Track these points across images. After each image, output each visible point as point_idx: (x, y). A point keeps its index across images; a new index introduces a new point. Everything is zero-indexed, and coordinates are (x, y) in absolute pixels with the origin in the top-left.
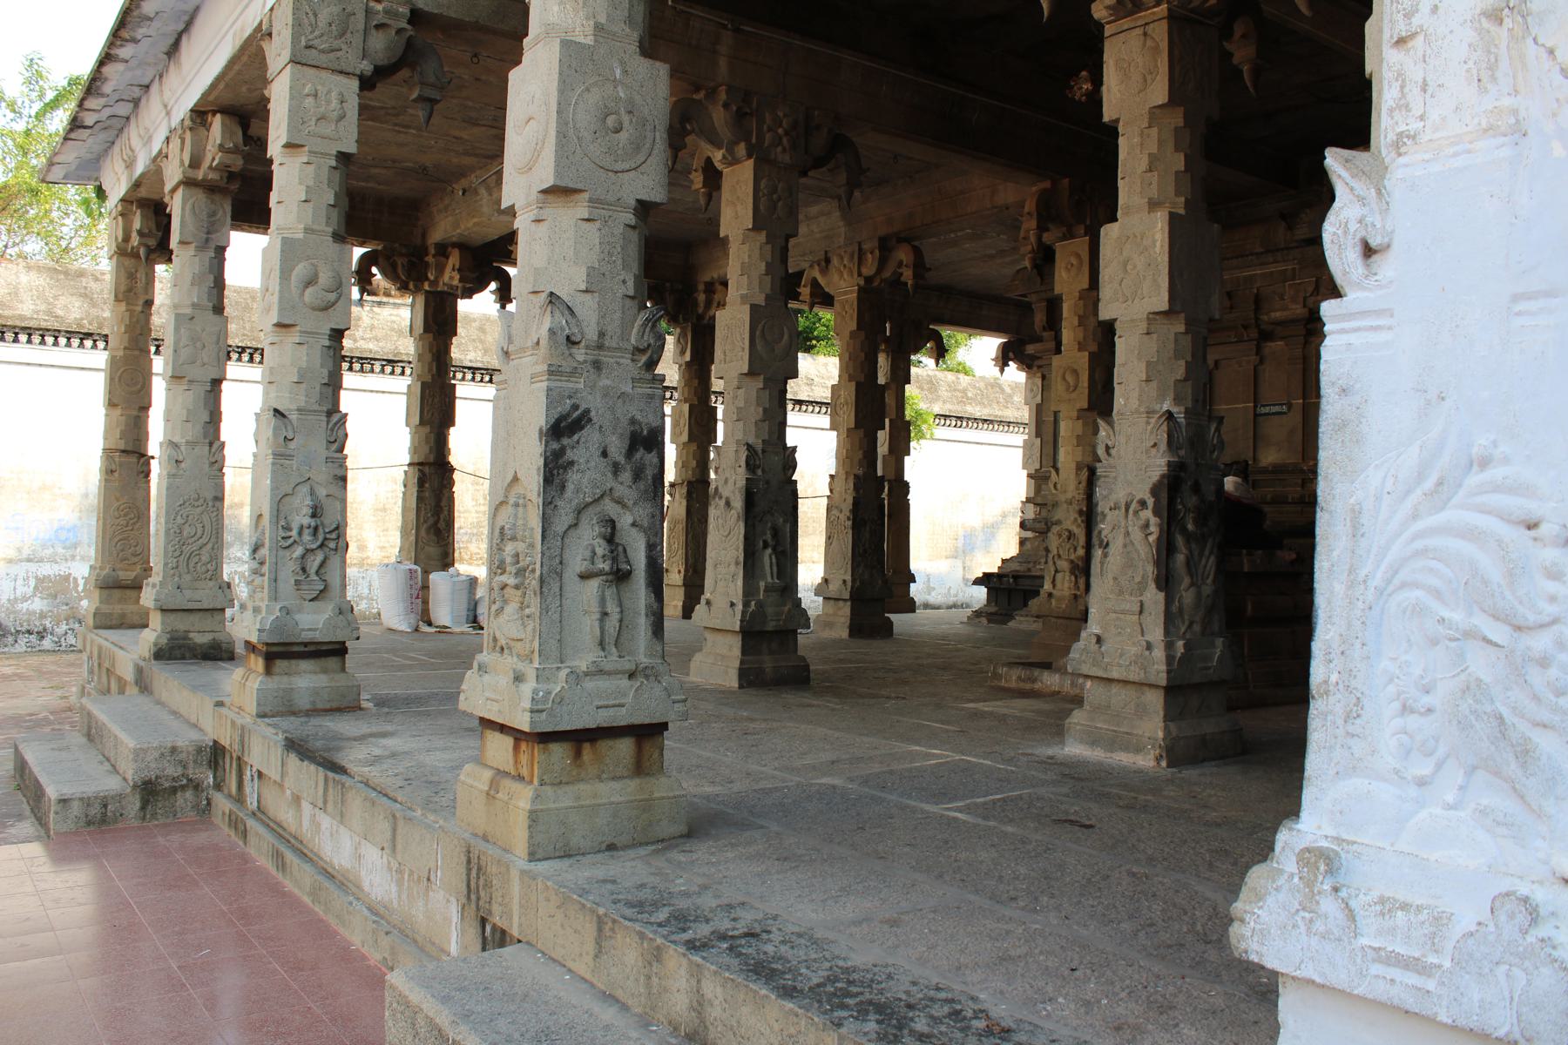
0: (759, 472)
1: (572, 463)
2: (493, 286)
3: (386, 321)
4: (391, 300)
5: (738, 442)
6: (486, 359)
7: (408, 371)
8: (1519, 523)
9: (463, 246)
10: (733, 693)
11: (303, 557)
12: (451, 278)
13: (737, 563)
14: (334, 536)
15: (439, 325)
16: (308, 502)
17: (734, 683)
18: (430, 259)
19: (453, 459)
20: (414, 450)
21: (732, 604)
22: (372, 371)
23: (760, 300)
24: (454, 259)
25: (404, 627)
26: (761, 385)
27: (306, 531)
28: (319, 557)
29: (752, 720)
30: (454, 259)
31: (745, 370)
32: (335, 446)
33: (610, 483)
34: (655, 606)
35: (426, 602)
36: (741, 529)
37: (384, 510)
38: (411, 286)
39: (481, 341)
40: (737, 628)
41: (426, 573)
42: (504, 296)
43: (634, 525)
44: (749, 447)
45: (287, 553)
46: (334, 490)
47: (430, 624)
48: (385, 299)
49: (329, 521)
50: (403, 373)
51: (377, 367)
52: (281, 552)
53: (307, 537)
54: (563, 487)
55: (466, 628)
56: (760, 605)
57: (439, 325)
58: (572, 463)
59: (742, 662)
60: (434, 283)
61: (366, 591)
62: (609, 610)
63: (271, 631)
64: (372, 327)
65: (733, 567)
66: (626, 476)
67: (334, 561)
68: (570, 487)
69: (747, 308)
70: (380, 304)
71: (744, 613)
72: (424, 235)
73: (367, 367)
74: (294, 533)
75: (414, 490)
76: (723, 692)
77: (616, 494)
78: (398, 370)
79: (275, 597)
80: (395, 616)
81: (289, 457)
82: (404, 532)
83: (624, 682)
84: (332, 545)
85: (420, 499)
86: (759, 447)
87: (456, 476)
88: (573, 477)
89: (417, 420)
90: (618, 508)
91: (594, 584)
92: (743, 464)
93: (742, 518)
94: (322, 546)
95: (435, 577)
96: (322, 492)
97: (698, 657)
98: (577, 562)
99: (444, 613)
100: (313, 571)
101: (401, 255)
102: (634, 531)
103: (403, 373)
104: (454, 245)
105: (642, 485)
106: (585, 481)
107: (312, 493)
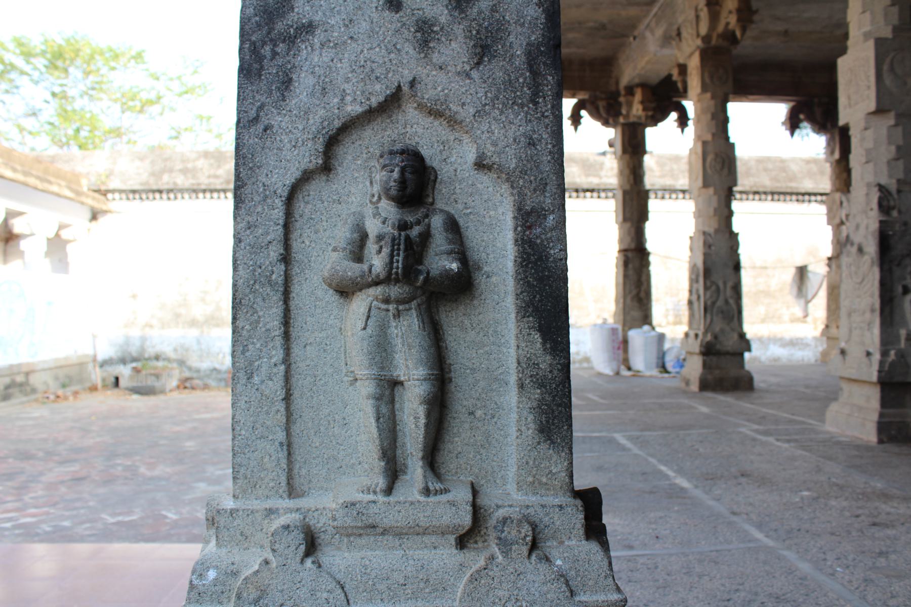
0: (895, 213)
1: (309, 28)
3: (588, 142)
5: (868, 185)
8: (870, 360)
9: (643, 86)
10: (868, 448)
12: (638, 110)
13: (873, 311)
15: (633, 148)
17: (870, 435)
18: (622, 99)
19: (649, 246)
20: (621, 241)
21: (868, 354)
23: (887, 33)
24: (638, 95)
25: (608, 371)
26: (892, 122)
29: (885, 496)
31: (872, 106)
33: (408, 65)
34: (545, 361)
36: (875, 275)
38: (611, 121)
40: (875, 378)
42: (683, 121)
43: (481, 165)
44: (881, 188)
47: (629, 369)
54: (286, 83)
55: (655, 372)
56: (901, 355)
57: (633, 148)
58: (309, 28)
59: (881, 415)
60: (627, 116)
62: (401, 373)
65: (868, 315)
66: (455, 50)
68: (304, 82)
69: (871, 44)
71: (882, 363)
72: (617, 83)
76: (858, 447)
77: (428, 94)
80: (602, 364)
82: (617, 301)
83: (446, 555)
85: (626, 276)
86: (893, 186)
88: (311, 60)
89: (621, 218)
90: (439, 128)
91: (360, 304)
92: (875, 205)
93: (877, 262)
97: (834, 407)
98: (323, 252)
99: (640, 360)
101: (602, 99)
102: (485, 181)
104: (638, 85)
105: (496, 69)
106: (344, 67)
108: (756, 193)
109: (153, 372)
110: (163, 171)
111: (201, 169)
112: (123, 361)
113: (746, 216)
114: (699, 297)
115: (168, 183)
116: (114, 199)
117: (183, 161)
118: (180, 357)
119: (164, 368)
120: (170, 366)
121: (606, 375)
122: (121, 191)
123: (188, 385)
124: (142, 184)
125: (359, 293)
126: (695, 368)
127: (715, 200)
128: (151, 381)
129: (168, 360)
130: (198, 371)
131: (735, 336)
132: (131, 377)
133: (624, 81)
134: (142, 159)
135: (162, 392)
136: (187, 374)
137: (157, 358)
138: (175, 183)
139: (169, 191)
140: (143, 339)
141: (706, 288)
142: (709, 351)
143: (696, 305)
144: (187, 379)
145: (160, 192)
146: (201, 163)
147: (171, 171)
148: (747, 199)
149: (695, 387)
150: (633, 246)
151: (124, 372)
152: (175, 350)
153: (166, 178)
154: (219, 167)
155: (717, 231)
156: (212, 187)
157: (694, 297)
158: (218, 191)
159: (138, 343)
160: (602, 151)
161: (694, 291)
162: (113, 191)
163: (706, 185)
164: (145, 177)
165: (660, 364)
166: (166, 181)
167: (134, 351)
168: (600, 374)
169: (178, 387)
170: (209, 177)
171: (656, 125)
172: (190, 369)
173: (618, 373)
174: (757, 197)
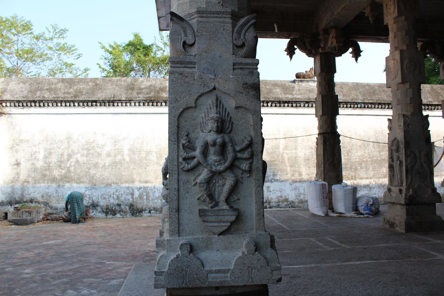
2: (350, 50)
4: (306, 79)
6: (344, 98)
7: (314, 105)
11: (209, 181)
12: (332, 43)
14: (246, 155)
16: (213, 114)
19: (339, 130)
22: (300, 106)
24: (333, 33)
25: (320, 213)
27: (212, 150)
28: (229, 181)
30: (333, 33)
32: (243, 51)
35: (330, 199)
37: (308, 160)
38: (313, 52)
39: (342, 92)
41: (330, 185)
45: (191, 177)
46: (244, 100)
48: (303, 79)
49: (241, 137)
50: (312, 106)
51: (302, 105)
52: (184, 177)
53: (213, 157)
55: (352, 214)
60: (324, 48)
61: (303, 191)
63: (169, 274)
64: (299, 90)
67: (249, 185)
70: (301, 81)
73: (298, 105)
74: (197, 153)
75: (321, 147)
78: (310, 105)
79: (177, 230)
81: (191, 64)
84: (245, 166)
85: (324, 150)
87: (341, 138)
94: (232, 167)
95: (334, 187)
96: (230, 104)
99: (340, 206)
100: (222, 198)
103: (312, 106)
104: (332, 28)
107: (218, 103)
108: (379, 104)
109: (27, 210)
110: (37, 90)
111: (60, 89)
112: (10, 203)
113: (177, 164)
114: (401, 163)
115: (39, 97)
116: (6, 106)
117: (49, 84)
118: (45, 201)
119: (34, 208)
120: (39, 206)
121: (320, 216)
122: (10, 101)
123: (49, 218)
124: (23, 97)
125: (362, 185)
126: (398, 214)
127: (410, 92)
128: (25, 216)
129: (38, 202)
130: (56, 209)
131: (429, 190)
132: (13, 214)
133: (323, 25)
134: (24, 83)
135: (32, 222)
136: (50, 211)
137: (31, 201)
138: (43, 97)
139: (40, 101)
140: (23, 189)
141: (407, 156)
142: (411, 203)
143: (397, 169)
144: (50, 214)
145: (35, 102)
146: (59, 86)
147: (42, 90)
148: (375, 108)
149: (401, 229)
150: (329, 130)
151: (10, 209)
152: (42, 196)
153: (38, 94)
154: (71, 87)
155: (412, 114)
156: (66, 99)
157: (396, 164)
158: (69, 102)
159: (20, 193)
160: (293, 80)
161: (395, 158)
162: (6, 101)
163: (403, 82)
164: (25, 93)
165: (355, 208)
166: (38, 96)
167: (17, 197)
168: (314, 215)
169: (43, 218)
170: (64, 93)
171: (341, 56)
172: (51, 208)
173: (327, 215)
174: (380, 106)
